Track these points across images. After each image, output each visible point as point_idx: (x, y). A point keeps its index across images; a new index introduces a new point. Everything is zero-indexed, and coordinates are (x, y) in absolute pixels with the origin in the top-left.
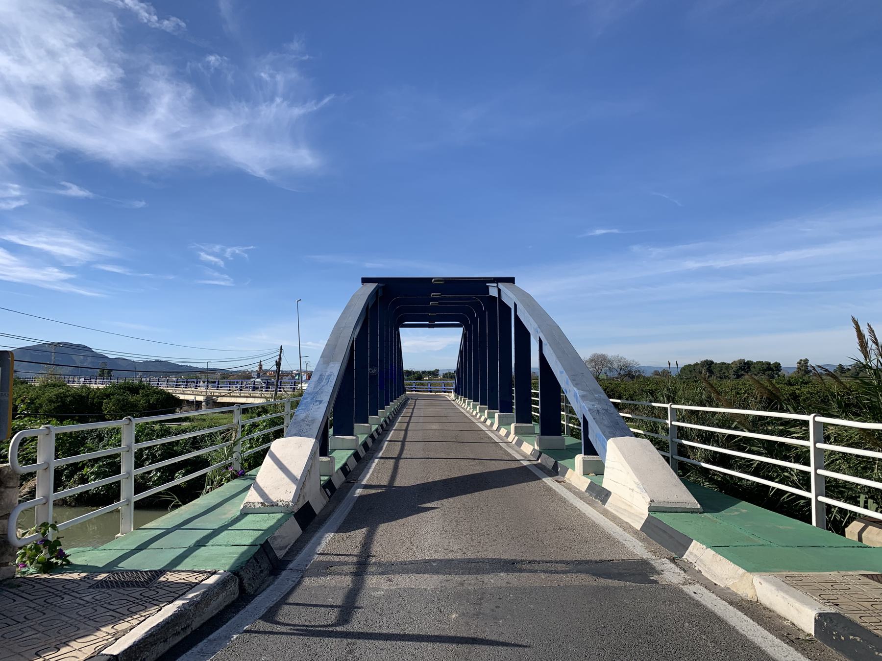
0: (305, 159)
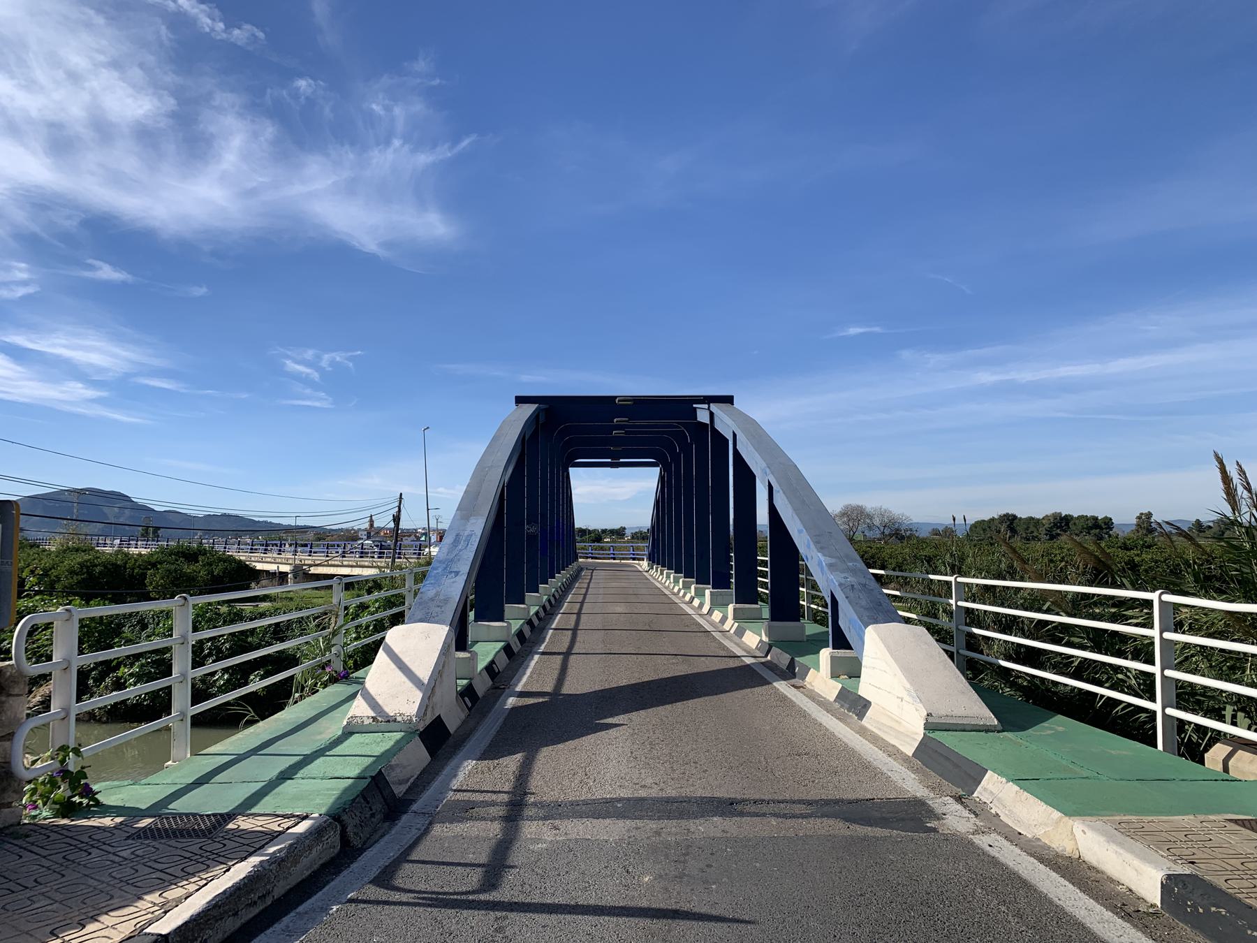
0: (434, 226)
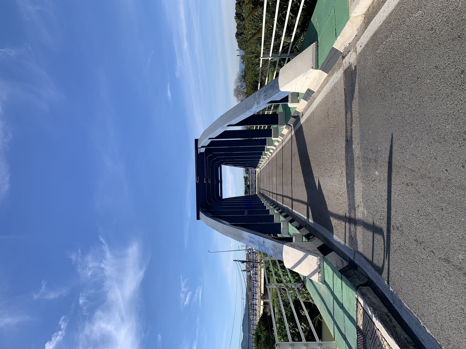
0: (133, 251)
